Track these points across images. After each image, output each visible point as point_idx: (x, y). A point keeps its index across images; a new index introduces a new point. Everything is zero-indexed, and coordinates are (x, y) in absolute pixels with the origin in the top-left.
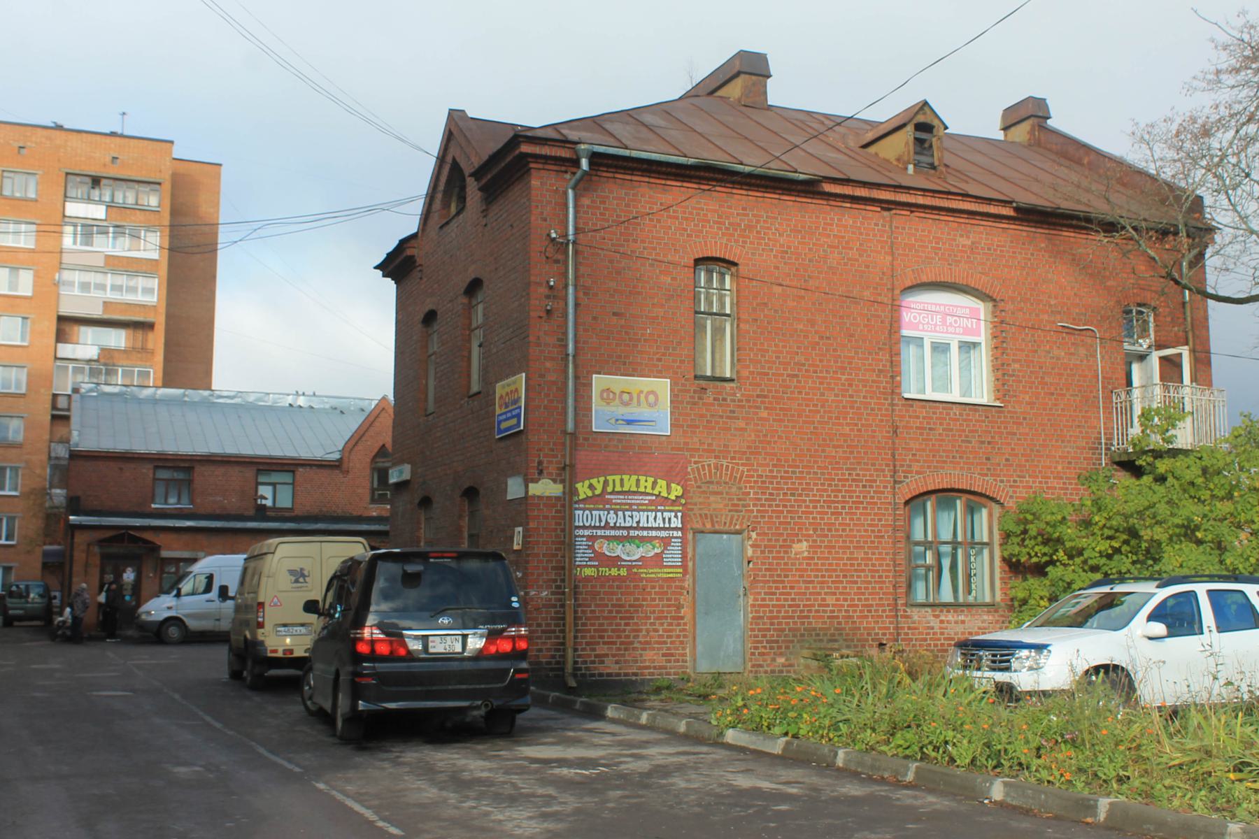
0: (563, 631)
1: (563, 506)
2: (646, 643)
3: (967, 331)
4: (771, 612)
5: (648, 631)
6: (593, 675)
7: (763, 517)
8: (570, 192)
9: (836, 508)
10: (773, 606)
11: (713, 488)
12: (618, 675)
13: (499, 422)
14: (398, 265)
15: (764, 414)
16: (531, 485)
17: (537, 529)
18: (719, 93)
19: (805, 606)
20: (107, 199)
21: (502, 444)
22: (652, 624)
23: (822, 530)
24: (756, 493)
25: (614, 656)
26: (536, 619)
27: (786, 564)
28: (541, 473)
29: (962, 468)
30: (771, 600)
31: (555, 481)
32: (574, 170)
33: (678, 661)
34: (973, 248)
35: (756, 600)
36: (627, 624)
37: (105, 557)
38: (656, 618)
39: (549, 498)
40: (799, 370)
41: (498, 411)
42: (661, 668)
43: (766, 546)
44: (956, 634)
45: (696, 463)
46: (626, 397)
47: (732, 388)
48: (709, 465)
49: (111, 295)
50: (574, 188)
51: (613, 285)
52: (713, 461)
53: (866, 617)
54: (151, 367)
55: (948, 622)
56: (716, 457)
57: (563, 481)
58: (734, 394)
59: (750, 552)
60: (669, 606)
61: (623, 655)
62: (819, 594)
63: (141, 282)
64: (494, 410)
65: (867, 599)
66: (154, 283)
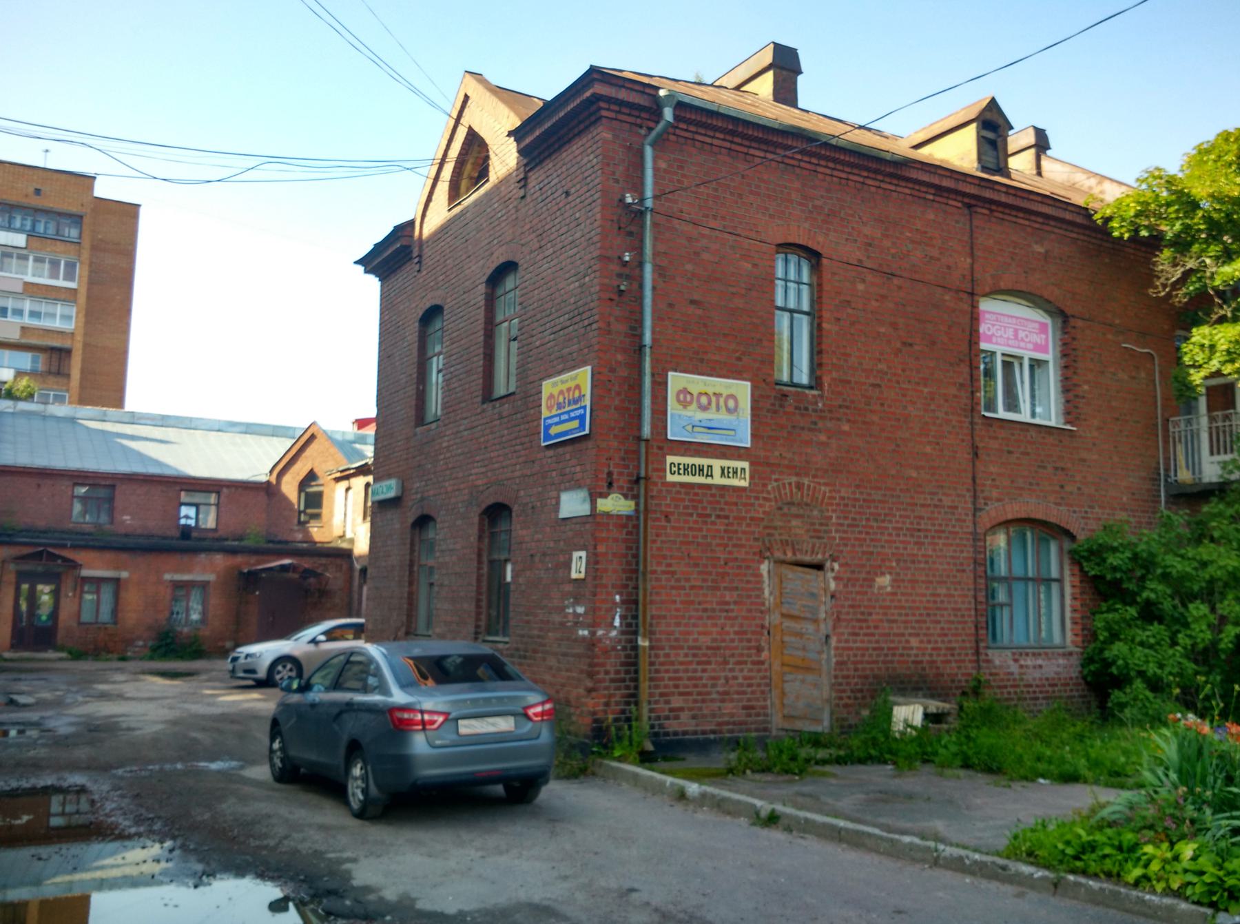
0: (636, 680)
1: (637, 527)
2: (726, 693)
3: (1037, 348)
4: (855, 656)
5: (727, 679)
6: (667, 734)
7: (846, 545)
8: (649, 151)
9: (919, 537)
10: (858, 649)
11: (794, 510)
12: (695, 733)
13: (548, 428)
14: (392, 257)
15: (846, 428)
16: (600, 501)
17: (605, 554)
18: (743, 89)
19: (889, 649)
20: (28, 228)
21: (550, 453)
22: (731, 670)
23: (905, 561)
24: (838, 518)
25: (691, 709)
26: (603, 665)
27: (870, 600)
28: (610, 485)
29: (1038, 497)
30: (855, 642)
31: (626, 497)
32: (651, 124)
33: (758, 715)
34: (1046, 256)
35: (839, 641)
36: (704, 671)
37: (22, 577)
38: (737, 663)
39: (619, 517)
40: (882, 379)
41: (545, 413)
42: (741, 723)
43: (849, 580)
44: (1034, 679)
45: (776, 480)
46: (704, 400)
47: (814, 396)
48: (790, 484)
49: (27, 320)
50: (653, 145)
51: (689, 267)
52: (794, 479)
53: (949, 662)
54: (67, 391)
55: (1027, 667)
56: (797, 475)
57: (635, 497)
58: (816, 403)
59: (833, 585)
60: (749, 648)
61: (700, 709)
62: (903, 635)
63: (59, 309)
64: (540, 412)
65: (950, 642)
66: (73, 311)
